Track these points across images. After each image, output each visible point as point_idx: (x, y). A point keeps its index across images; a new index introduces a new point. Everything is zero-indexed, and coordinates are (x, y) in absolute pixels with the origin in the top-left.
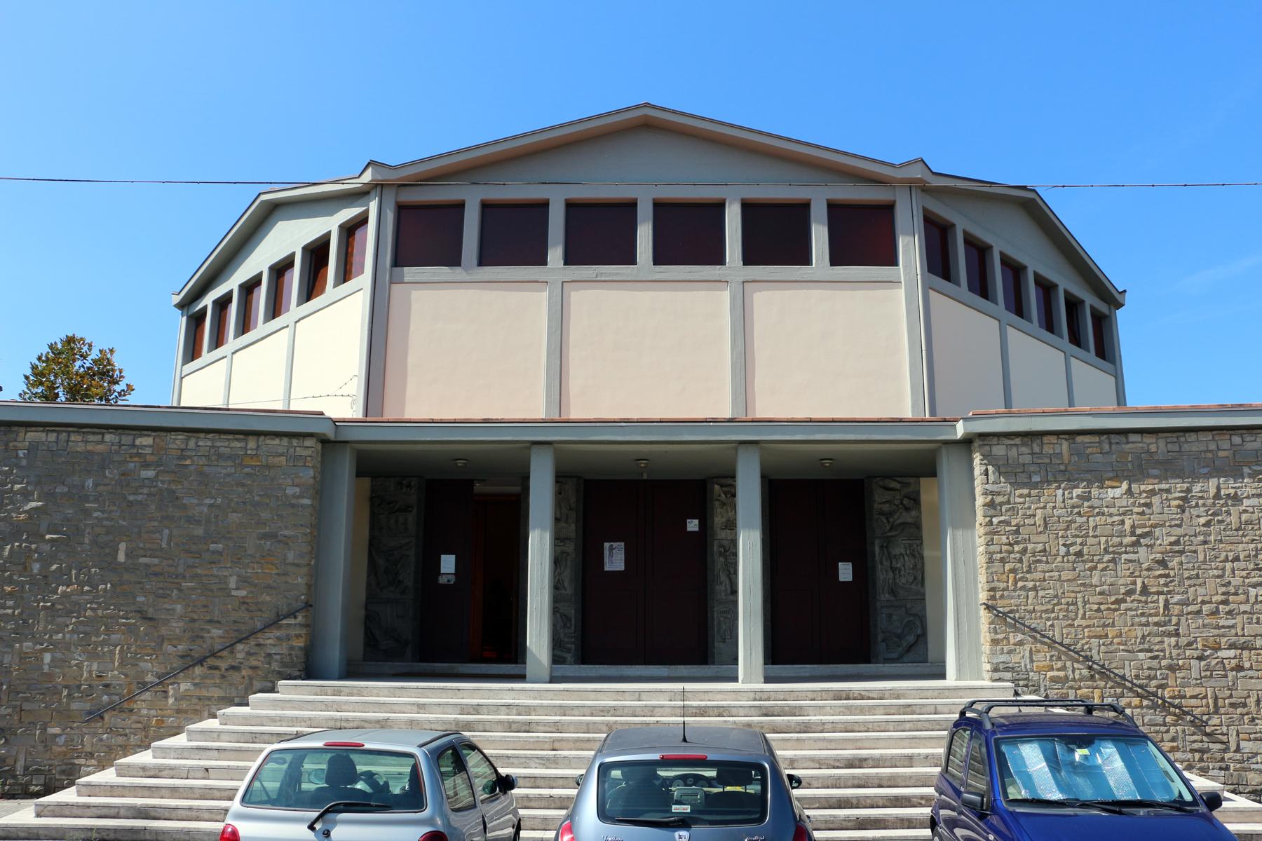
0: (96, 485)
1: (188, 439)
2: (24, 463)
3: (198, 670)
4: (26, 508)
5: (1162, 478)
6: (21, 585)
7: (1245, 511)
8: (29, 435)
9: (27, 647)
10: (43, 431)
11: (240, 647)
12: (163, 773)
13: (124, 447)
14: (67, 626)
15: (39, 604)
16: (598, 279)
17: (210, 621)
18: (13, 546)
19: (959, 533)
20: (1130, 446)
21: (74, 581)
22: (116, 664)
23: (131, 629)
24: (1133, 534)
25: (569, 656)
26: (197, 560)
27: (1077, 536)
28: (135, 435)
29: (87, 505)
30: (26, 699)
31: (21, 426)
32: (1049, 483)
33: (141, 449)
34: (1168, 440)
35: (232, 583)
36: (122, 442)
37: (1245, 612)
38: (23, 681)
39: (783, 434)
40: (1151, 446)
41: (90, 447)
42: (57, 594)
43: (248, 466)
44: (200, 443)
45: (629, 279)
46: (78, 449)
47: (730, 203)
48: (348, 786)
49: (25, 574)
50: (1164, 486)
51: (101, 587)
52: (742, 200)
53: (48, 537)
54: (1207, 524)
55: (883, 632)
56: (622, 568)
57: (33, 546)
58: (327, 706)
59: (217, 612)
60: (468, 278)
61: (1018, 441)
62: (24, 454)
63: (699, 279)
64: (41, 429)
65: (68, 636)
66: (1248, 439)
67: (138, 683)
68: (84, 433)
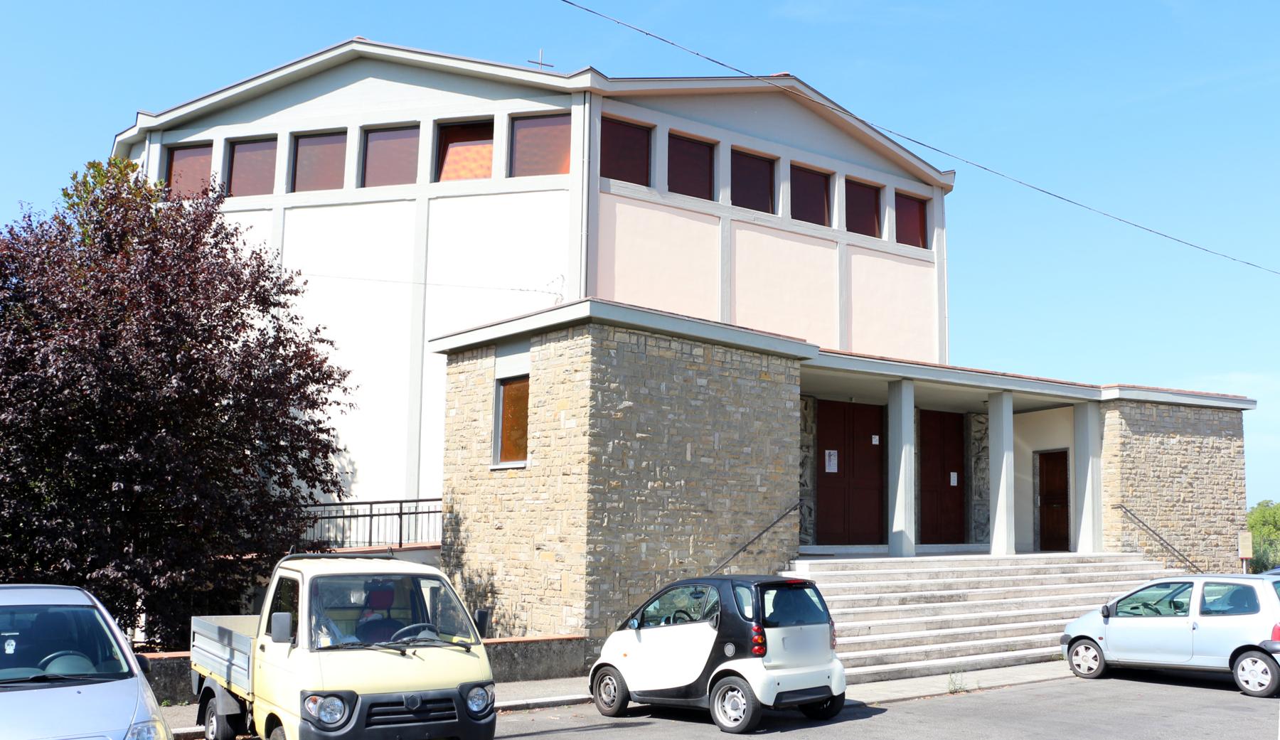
0: (668, 389)
1: (725, 353)
2: (615, 363)
3: (741, 555)
4: (621, 407)
5: (1192, 435)
6: (622, 479)
7: (1222, 457)
8: (618, 335)
9: (630, 538)
10: (626, 333)
12: (844, 633)
13: (685, 355)
14: (656, 518)
15: (636, 498)
16: (756, 222)
17: (746, 513)
18: (614, 443)
19: (1095, 460)
20: (1180, 413)
21: (658, 477)
22: (691, 552)
23: (699, 521)
24: (1181, 467)
26: (737, 461)
27: (1158, 466)
28: (691, 345)
29: (663, 407)
30: (631, 585)
31: (611, 326)
32: (1148, 432)
36: (684, 351)
37: (1220, 514)
38: (628, 569)
39: (1031, 388)
40: (1189, 415)
41: (662, 353)
42: (647, 489)
43: (764, 381)
44: (734, 358)
45: (776, 227)
46: (654, 354)
47: (839, 178)
49: (623, 470)
50: (1193, 439)
51: (677, 483)
52: (846, 176)
53: (638, 435)
54: (1208, 463)
55: (975, 522)
56: (836, 471)
57: (629, 444)
58: (888, 576)
59: (750, 506)
60: (661, 201)
61: (1135, 405)
63: (820, 236)
64: (625, 330)
65: (657, 527)
67: (705, 567)
68: (656, 338)
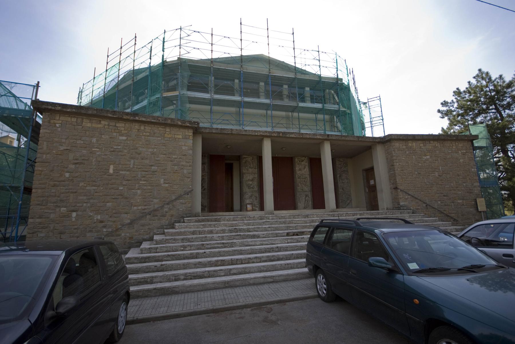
1: (140, 126)
11: (166, 206)
25: (257, 209)
33: (119, 128)
34: (440, 143)
35: (162, 181)
44: (146, 128)
48: (19, 247)
62: (59, 125)
66: (459, 143)
68: (90, 119)
